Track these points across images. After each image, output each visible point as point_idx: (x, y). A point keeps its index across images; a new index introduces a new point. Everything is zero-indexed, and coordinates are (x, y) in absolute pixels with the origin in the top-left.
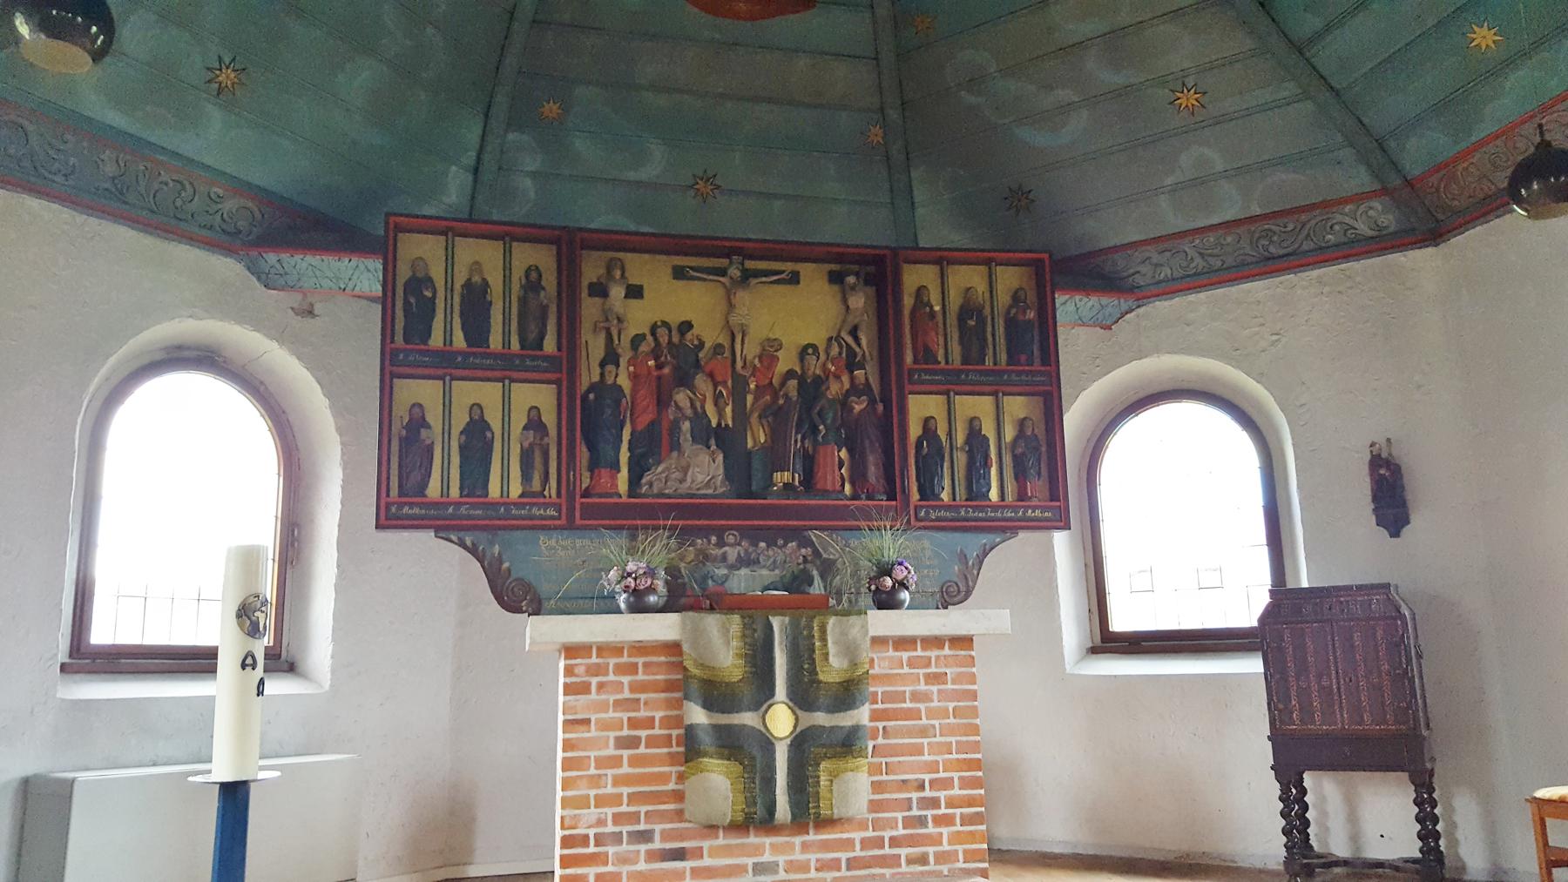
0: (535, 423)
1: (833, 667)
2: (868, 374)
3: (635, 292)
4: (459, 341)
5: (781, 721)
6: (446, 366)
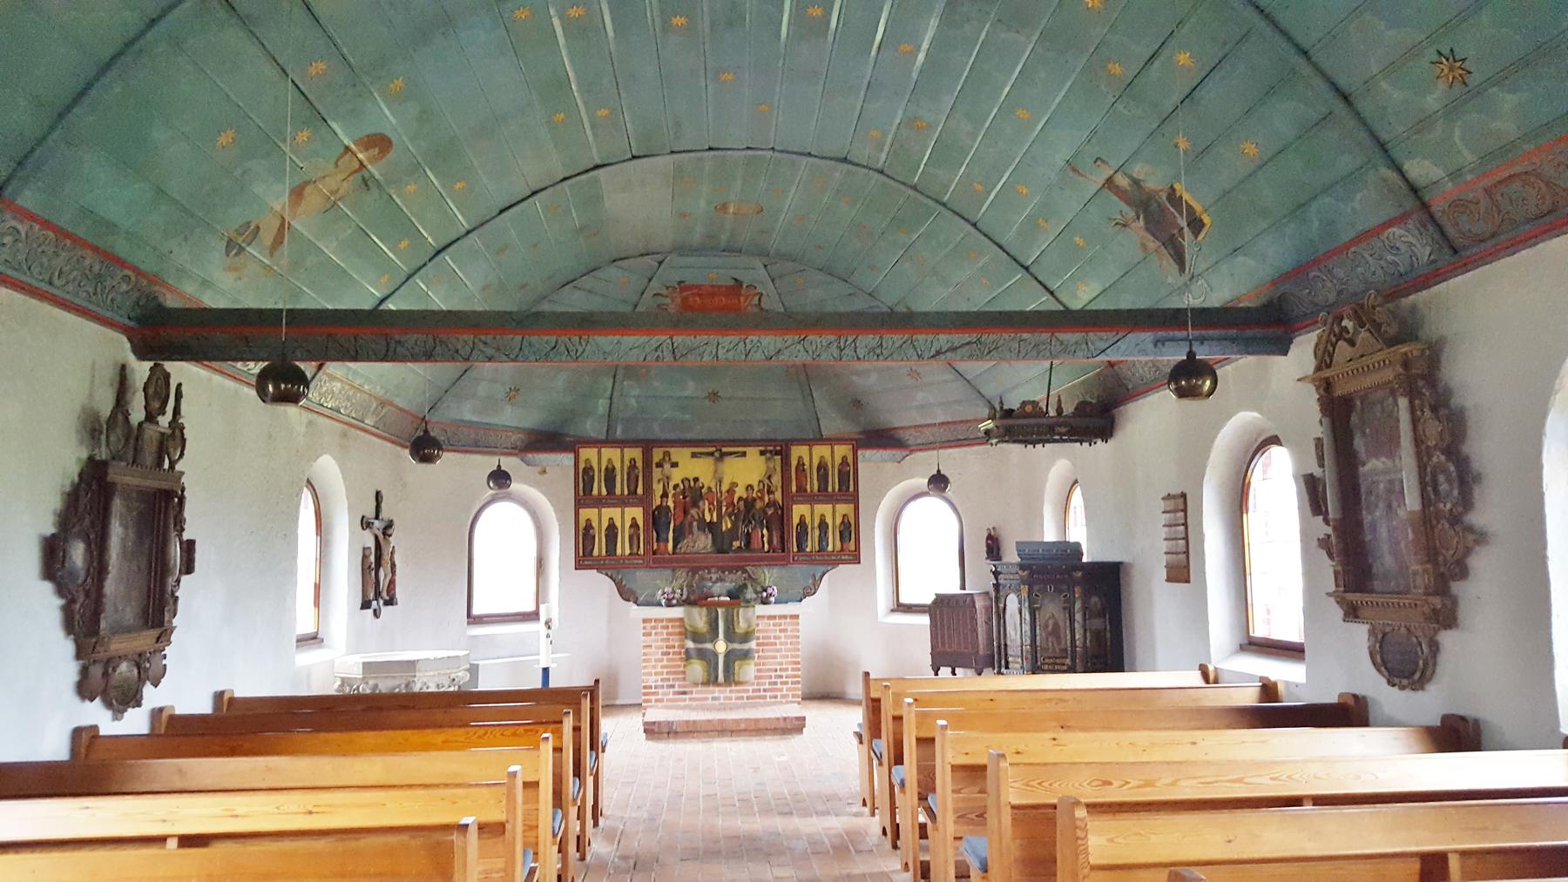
0: (634, 525)
1: (741, 626)
2: (778, 496)
3: (675, 465)
4: (604, 492)
5: (721, 647)
6: (599, 503)
